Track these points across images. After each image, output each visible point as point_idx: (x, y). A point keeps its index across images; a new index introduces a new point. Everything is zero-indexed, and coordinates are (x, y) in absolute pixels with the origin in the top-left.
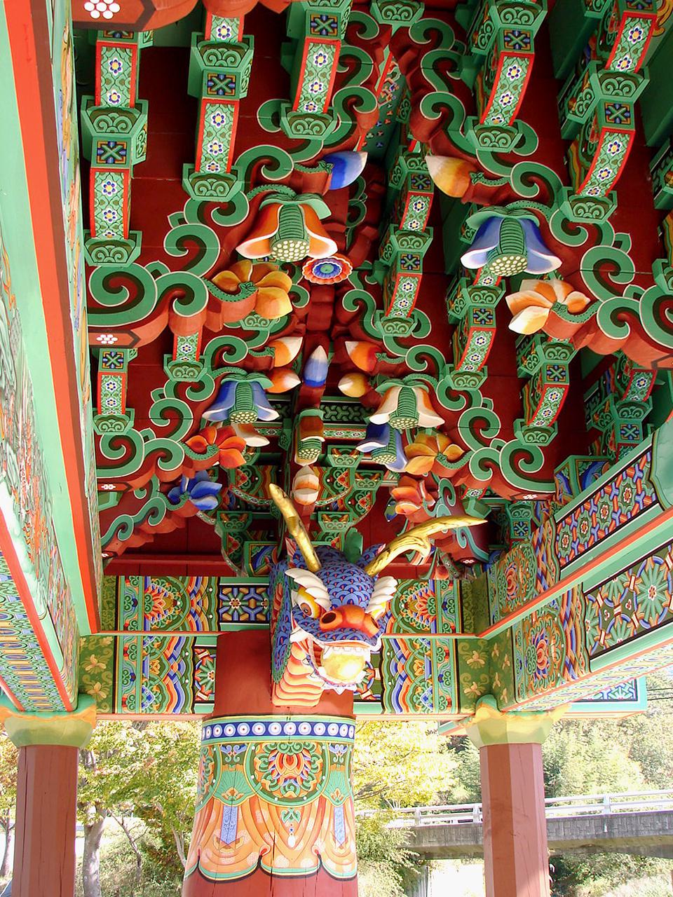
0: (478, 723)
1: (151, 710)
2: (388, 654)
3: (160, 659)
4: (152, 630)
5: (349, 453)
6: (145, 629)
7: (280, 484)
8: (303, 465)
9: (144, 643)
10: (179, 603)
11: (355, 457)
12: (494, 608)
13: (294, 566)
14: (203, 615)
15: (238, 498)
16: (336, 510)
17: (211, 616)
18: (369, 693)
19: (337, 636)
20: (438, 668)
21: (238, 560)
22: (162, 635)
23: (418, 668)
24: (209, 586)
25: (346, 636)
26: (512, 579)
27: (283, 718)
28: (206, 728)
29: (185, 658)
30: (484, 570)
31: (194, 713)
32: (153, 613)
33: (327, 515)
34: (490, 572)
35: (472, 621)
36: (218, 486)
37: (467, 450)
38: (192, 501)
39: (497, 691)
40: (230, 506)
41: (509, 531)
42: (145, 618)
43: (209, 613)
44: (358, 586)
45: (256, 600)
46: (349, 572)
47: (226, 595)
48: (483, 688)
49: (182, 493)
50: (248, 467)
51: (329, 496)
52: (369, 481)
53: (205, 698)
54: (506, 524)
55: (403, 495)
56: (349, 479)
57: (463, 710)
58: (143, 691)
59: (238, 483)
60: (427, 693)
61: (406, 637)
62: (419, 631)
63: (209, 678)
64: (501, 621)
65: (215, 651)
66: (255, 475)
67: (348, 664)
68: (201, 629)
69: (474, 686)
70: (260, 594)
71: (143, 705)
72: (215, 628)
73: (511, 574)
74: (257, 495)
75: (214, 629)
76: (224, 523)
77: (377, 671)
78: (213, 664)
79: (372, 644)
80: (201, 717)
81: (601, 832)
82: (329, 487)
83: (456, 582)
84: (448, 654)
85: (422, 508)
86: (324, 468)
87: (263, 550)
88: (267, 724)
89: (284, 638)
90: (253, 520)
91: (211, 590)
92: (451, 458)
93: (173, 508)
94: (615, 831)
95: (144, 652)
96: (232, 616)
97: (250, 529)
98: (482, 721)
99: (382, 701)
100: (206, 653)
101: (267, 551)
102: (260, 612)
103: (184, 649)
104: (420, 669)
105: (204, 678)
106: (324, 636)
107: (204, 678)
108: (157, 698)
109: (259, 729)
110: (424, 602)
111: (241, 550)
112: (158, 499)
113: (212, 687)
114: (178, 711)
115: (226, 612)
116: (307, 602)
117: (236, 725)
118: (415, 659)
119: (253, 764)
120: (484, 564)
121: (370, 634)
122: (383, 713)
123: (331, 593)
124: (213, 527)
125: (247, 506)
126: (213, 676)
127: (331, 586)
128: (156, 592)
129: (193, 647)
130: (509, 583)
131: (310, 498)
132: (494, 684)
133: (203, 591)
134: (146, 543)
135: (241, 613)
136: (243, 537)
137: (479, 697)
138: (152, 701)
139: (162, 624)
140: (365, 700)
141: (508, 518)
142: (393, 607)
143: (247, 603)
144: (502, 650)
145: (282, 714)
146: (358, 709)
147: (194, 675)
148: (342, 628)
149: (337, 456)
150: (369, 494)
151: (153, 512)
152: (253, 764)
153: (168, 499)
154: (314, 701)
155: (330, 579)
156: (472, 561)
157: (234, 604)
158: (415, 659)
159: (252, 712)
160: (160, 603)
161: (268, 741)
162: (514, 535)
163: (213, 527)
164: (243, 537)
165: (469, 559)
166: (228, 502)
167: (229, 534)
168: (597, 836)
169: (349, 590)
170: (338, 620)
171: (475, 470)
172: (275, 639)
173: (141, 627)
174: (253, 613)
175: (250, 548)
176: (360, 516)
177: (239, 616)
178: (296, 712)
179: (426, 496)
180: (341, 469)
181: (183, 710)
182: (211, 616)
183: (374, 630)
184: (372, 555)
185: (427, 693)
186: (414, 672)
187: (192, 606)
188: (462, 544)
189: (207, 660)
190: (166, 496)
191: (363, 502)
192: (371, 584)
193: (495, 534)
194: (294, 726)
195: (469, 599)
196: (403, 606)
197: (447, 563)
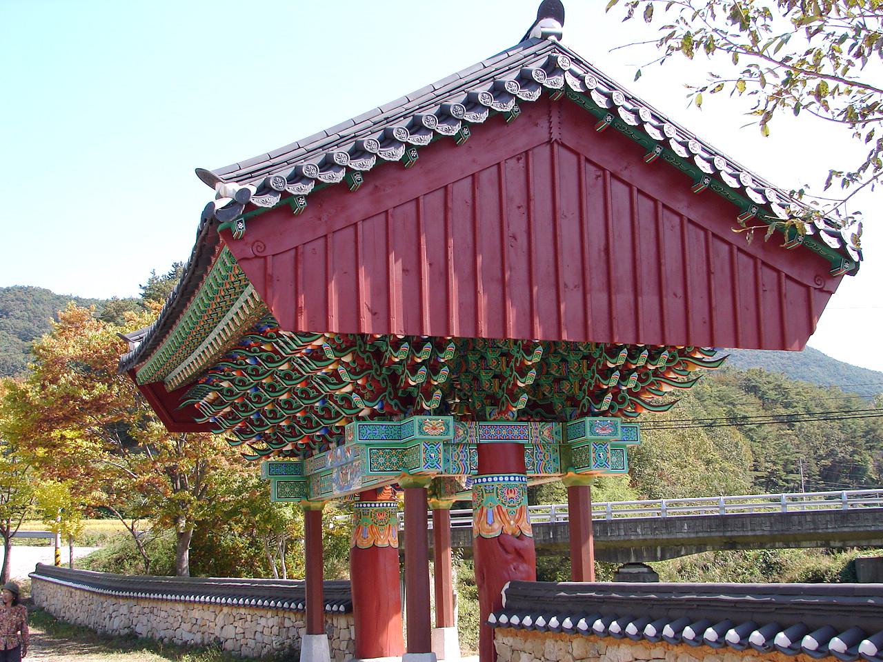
81: (547, 538)
88: (375, 504)
94: (559, 537)
109: (373, 505)
119: (497, 493)
152: (497, 493)
161: (375, 509)
168: (544, 541)
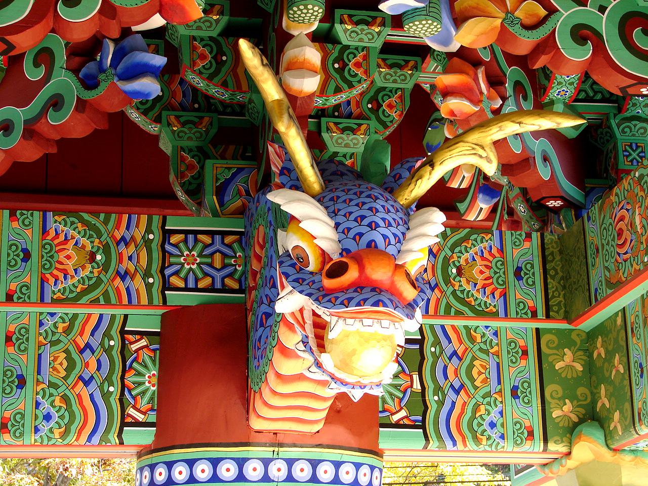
0: (576, 468)
1: (49, 439)
2: (433, 349)
3: (67, 351)
4: (56, 302)
5: (368, 24)
6: (42, 299)
7: (259, 43)
8: (295, 33)
9: (41, 324)
10: (99, 257)
11: (377, 30)
12: (597, 276)
13: (281, 186)
14: (138, 278)
15: (195, 90)
16: (349, 116)
17: (151, 280)
18: (403, 413)
19: (350, 300)
20: (511, 376)
21: (195, 191)
22: (71, 311)
23: (480, 373)
24: (149, 230)
25: (365, 300)
26: (624, 228)
27: (266, 452)
28: (141, 469)
29: (108, 350)
30: (578, 216)
31: (121, 443)
32: (56, 272)
33: (336, 124)
34: (589, 219)
35: (561, 299)
36: (160, 61)
37: (552, 11)
38: (118, 83)
39: (604, 414)
40: (180, 102)
41: (616, 157)
42: (43, 281)
43: (147, 274)
44: (384, 219)
45: (224, 255)
46: (369, 196)
47: (175, 246)
48: (583, 411)
49: (102, 70)
50: (211, 38)
51: (338, 90)
52: (399, 72)
53: (140, 417)
54: (611, 147)
55: (452, 87)
56: (368, 65)
57: (552, 446)
58: (38, 405)
59: (194, 64)
60: (494, 416)
61: (459, 323)
62: (481, 314)
63: (147, 384)
64: (608, 296)
65: (157, 338)
66: (220, 53)
67: (368, 350)
68: (135, 301)
69: (568, 407)
70: (229, 246)
71: (37, 430)
72: (157, 300)
73: (622, 219)
74: (224, 85)
75: (156, 302)
76: (173, 132)
77: (416, 377)
78: (154, 361)
79: (408, 316)
80: (134, 451)
82: (337, 76)
83: (535, 236)
84: (525, 353)
85: (482, 110)
86: (330, 46)
87: (234, 175)
88: (241, 462)
89: (268, 315)
90: (220, 129)
91: (151, 237)
92: (527, 21)
93: (89, 95)
95: (41, 338)
96: (186, 280)
97: (215, 142)
98: (583, 464)
99: (423, 427)
100: (143, 343)
101: (241, 177)
102: (230, 275)
103: (107, 335)
104: (483, 376)
105: (140, 384)
106: (329, 301)
107: (140, 384)
108: (62, 417)
110: (487, 266)
111: (201, 175)
112: (63, 80)
113: (152, 399)
114: (96, 439)
115: (176, 273)
116: (302, 244)
117: (191, 463)
118: (474, 358)
120: (576, 208)
121: (404, 299)
122: (425, 448)
123: (341, 228)
124: (156, 138)
125: (208, 103)
126: (155, 380)
127: (340, 219)
128: (62, 238)
129: (123, 332)
130: (620, 233)
131: (309, 84)
132: (599, 405)
133: (139, 238)
134: (46, 155)
135: (200, 275)
136: (202, 154)
137: (576, 425)
138: (52, 424)
139: (71, 291)
140: (397, 425)
141: (612, 136)
142: (439, 271)
143: (209, 260)
144: (610, 348)
145: (264, 445)
146: (387, 440)
147: (123, 378)
148: (357, 286)
149: (349, 27)
150: (399, 93)
151: (56, 103)
153: (78, 78)
154: (316, 422)
155: (338, 206)
156: (558, 203)
157: (189, 260)
158: (474, 358)
159: (217, 441)
160: (68, 257)
162: (623, 164)
163: (156, 138)
164: (202, 154)
165: (555, 198)
166: (180, 97)
167: (182, 148)
169: (370, 225)
170: (352, 274)
171: (564, 42)
172: (253, 318)
173: (35, 296)
174: (218, 275)
175: (215, 170)
176: (386, 127)
177: (197, 280)
178: (286, 441)
179: (488, 91)
180: (357, 49)
181: (104, 439)
182: (151, 280)
183: (410, 293)
184: (406, 174)
185: (494, 416)
186: (472, 380)
187: (121, 261)
188: (544, 173)
189: (145, 356)
190: (77, 76)
191: (390, 106)
192: (404, 217)
193: (591, 158)
194: (284, 466)
195: (555, 264)
196: (454, 271)
197: (521, 208)
